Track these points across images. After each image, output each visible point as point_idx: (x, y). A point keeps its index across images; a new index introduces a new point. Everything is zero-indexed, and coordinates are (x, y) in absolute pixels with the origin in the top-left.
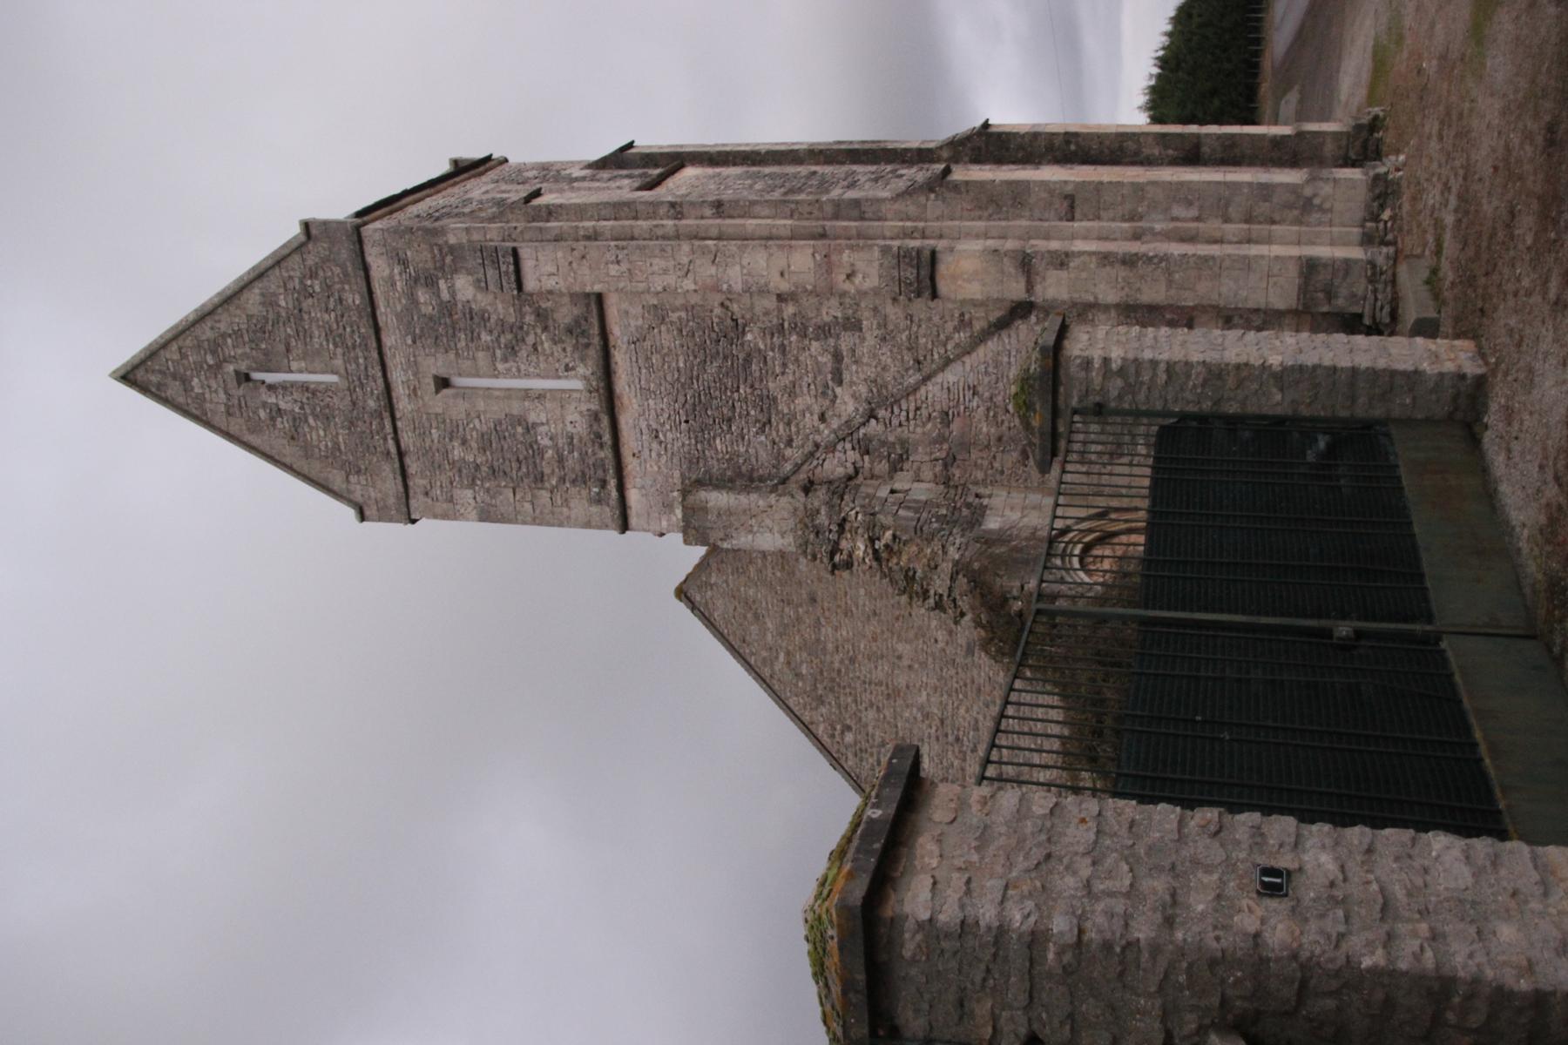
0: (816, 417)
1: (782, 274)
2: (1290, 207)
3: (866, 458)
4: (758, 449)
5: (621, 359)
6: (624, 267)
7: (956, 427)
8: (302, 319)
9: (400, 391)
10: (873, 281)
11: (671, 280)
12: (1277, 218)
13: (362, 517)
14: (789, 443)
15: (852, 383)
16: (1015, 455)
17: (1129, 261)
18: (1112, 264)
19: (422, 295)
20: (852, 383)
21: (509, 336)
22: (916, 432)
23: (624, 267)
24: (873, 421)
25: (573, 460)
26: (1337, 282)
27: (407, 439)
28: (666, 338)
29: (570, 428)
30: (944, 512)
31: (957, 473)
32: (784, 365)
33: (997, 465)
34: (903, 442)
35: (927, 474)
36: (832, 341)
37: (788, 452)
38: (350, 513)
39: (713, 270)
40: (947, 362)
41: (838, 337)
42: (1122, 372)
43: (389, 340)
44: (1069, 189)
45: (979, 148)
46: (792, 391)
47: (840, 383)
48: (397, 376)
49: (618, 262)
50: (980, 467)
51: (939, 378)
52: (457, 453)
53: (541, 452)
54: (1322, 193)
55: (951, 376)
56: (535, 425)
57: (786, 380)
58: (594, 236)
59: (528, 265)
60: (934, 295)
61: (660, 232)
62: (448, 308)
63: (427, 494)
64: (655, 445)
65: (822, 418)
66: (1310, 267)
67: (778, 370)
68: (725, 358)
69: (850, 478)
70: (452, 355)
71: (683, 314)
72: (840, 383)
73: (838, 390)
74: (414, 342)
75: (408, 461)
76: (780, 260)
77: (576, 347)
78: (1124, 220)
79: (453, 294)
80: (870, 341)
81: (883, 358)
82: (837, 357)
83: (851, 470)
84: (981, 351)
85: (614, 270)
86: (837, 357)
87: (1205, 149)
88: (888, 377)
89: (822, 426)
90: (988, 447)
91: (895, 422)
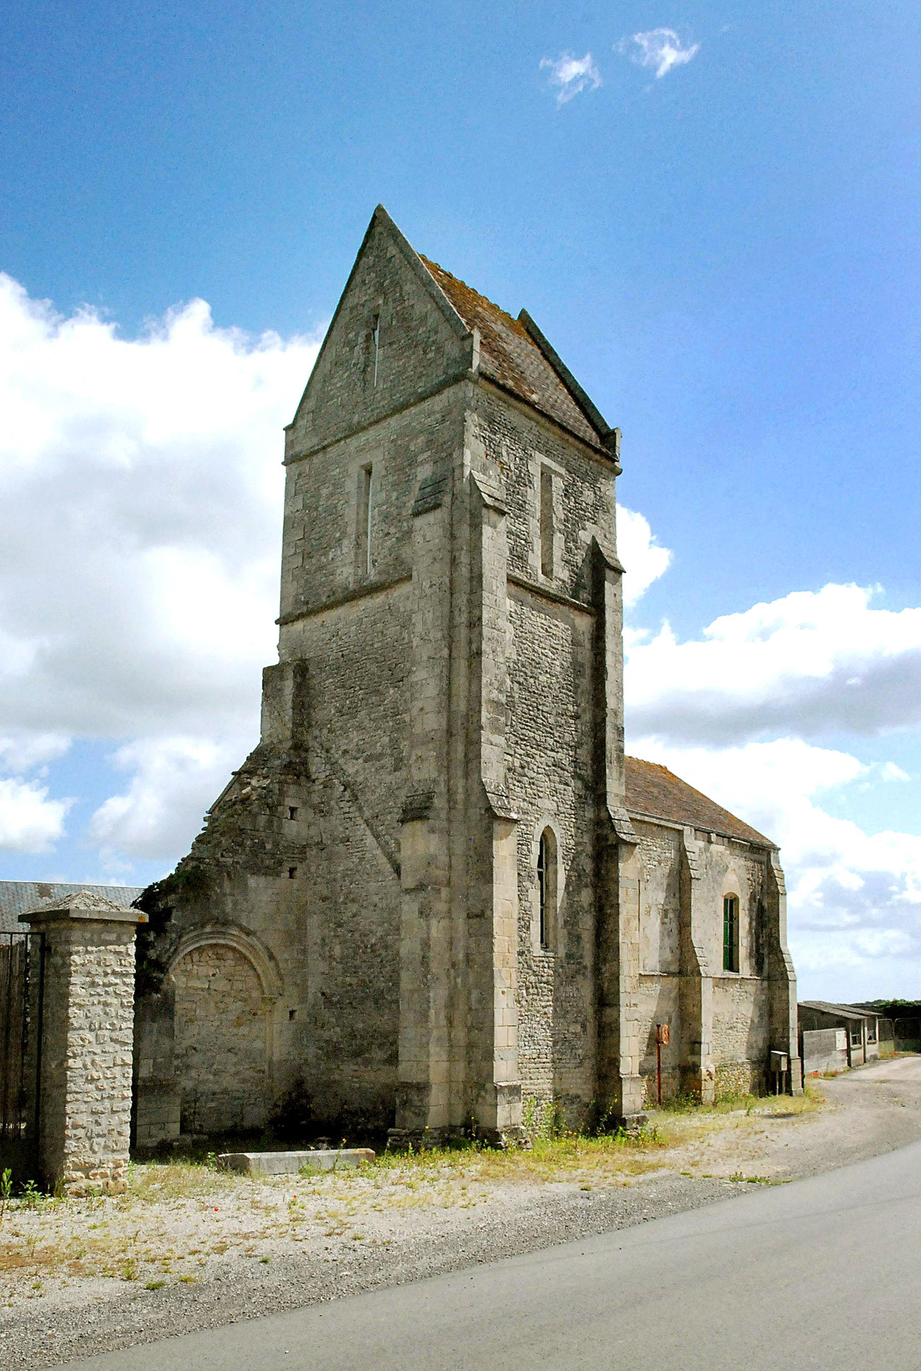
0: (345, 747)
1: (422, 709)
2: (479, 1074)
3: (321, 787)
4: (326, 711)
5: (379, 599)
6: (428, 591)
7: (341, 848)
8: (410, 348)
9: (362, 438)
10: (417, 775)
11: (419, 628)
12: (473, 1065)
13: (287, 429)
14: (330, 731)
15: (365, 769)
16: (325, 893)
17: (424, 961)
18: (422, 949)
19: (421, 440)
20: (365, 769)
21: (395, 514)
22: (336, 820)
23: (428, 591)
24: (342, 788)
25: (320, 578)
26: (413, 1109)
27: (333, 452)
28: (393, 630)
29: (339, 571)
30: (269, 847)
31: (314, 853)
32: (374, 720)
33: (319, 880)
34: (329, 813)
35: (313, 831)
36: (389, 751)
37: (325, 731)
38: (290, 421)
39: (425, 658)
40: (377, 837)
41: (392, 755)
42: (64, 964)
43: (393, 422)
44: (488, 912)
45: (607, 840)
46: (360, 728)
47: (366, 761)
48: (372, 433)
49: (431, 586)
50: (318, 868)
51: (368, 832)
52: (324, 492)
53: (325, 554)
54: (487, 1097)
55: (370, 840)
56: (340, 546)
57: (367, 723)
58: (454, 562)
59: (431, 517)
60: (403, 821)
61: (456, 613)
62: (413, 463)
63: (300, 474)
64: (328, 636)
65: (345, 752)
66: (422, 1088)
67: (373, 716)
68: (379, 677)
69: (308, 777)
70: (384, 473)
71: (406, 641)
72: (366, 761)
73: (361, 761)
74: (392, 441)
75: (320, 455)
76: (431, 705)
77: (387, 565)
78: (467, 955)
79: (422, 463)
80: (389, 779)
81: (378, 790)
82: (379, 757)
83: (313, 777)
84: (385, 860)
85: (426, 584)
86: (379, 757)
87: (608, 1011)
88: (369, 796)
89: (340, 752)
90: (330, 872)
91: (342, 804)
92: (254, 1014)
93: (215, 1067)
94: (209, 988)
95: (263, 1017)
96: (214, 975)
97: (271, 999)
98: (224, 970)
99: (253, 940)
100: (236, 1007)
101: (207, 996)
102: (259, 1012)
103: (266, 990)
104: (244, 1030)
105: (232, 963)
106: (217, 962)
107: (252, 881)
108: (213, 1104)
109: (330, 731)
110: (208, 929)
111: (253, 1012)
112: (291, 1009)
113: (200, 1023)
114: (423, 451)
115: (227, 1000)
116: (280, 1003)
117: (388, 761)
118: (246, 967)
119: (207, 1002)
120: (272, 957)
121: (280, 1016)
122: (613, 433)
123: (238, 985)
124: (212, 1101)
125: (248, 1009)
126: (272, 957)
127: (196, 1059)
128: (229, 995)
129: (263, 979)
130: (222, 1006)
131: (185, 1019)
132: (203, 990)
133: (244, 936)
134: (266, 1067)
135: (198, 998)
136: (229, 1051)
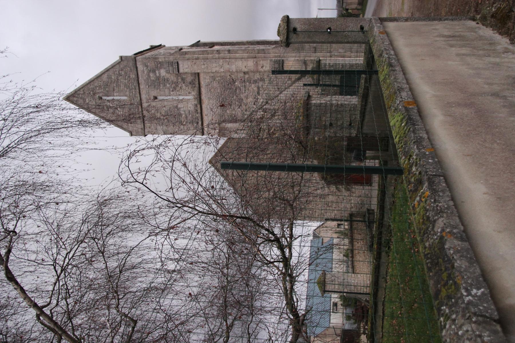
5: (203, 90)
6: (206, 66)
13: (132, 135)
19: (151, 75)
23: (206, 66)
28: (215, 84)
29: (189, 109)
43: (142, 87)
64: (211, 112)
76: (245, 63)
77: (192, 87)
85: (203, 67)
91: (273, 104)
109: (246, 110)
114: (156, 74)
117: (261, 84)
122: (121, 57)
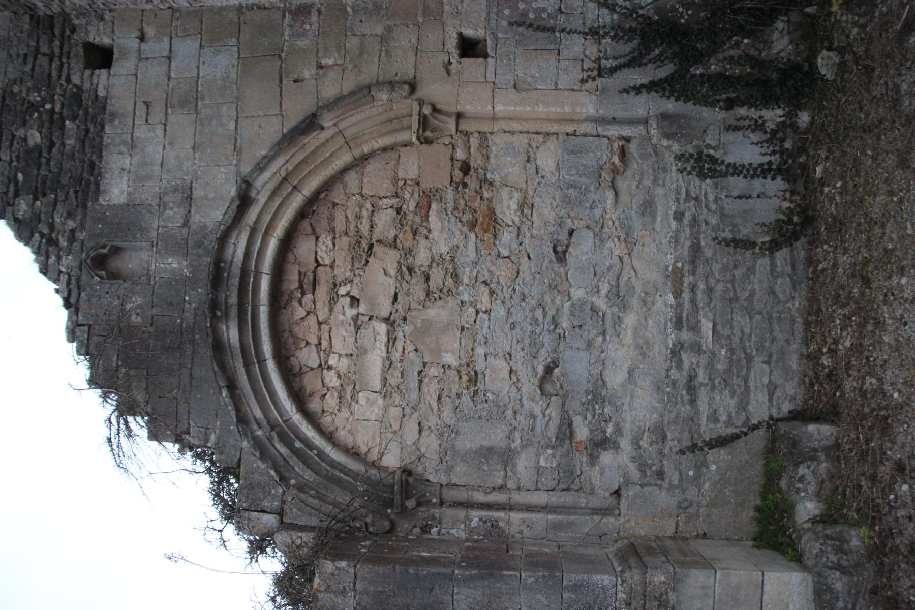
92: (466, 168)
93: (601, 304)
94: (386, 320)
95: (474, 141)
96: (355, 301)
97: (424, 122)
98: (342, 271)
99: (264, 183)
100: (442, 235)
101: (408, 329)
102: (460, 154)
103: (404, 136)
104: (508, 208)
105: (326, 239)
106: (322, 291)
107: (116, 191)
108: (707, 327)
110: (231, 334)
111: (458, 174)
112: (455, 53)
113: (480, 351)
115: (422, 258)
116: (436, 90)
118: (337, 195)
119: (427, 325)
120: (311, 124)
121: (470, 92)
123: (385, 219)
124: (695, 328)
125: (450, 194)
126: (311, 124)
127: (577, 367)
128: (409, 252)
129: (366, 149)
130: (437, 276)
131: (466, 399)
132: (391, 340)
133: (252, 215)
134: (614, 131)
135: (413, 355)
136: (561, 256)
